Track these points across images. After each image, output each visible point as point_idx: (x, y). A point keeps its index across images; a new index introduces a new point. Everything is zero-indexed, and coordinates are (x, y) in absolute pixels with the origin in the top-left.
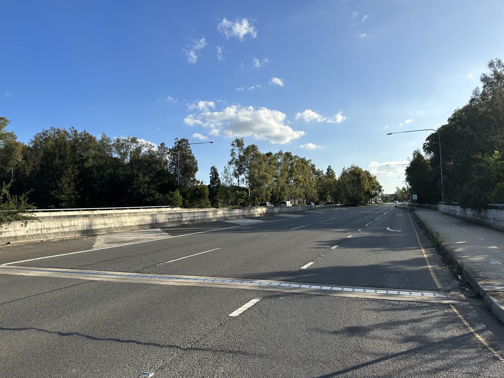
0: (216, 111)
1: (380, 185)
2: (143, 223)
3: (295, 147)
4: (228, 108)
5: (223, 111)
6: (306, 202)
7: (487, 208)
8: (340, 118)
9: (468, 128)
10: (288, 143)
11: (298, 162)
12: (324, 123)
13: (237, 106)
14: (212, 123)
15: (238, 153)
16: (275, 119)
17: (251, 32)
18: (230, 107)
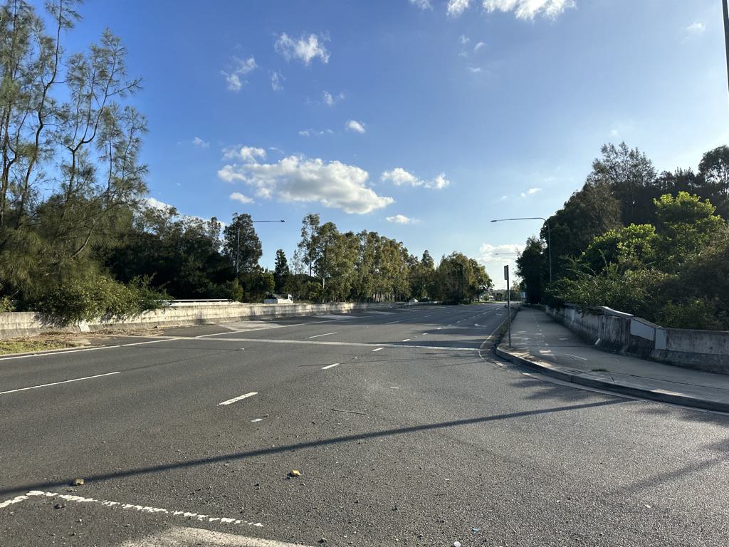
0: (267, 163)
1: (490, 278)
2: (244, 315)
4: (285, 160)
5: (277, 163)
6: (395, 297)
8: (441, 182)
9: (565, 226)
10: (370, 213)
11: (385, 245)
12: (421, 189)
13: (298, 158)
14: (260, 179)
15: (310, 232)
16: (352, 178)
17: (320, 55)
18: (288, 158)
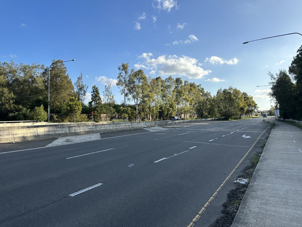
1: (256, 103)
3: (205, 80)
4: (160, 57)
12: (225, 64)
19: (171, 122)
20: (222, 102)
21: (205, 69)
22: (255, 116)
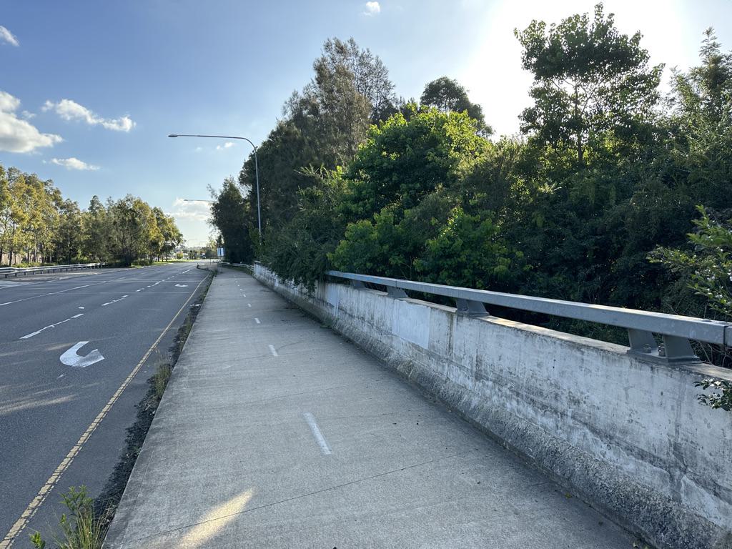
1: (180, 232)
3: (44, 162)
7: (327, 280)
12: (99, 128)
19: (16, 271)
20: (117, 229)
21: (42, 130)
22: (177, 260)
